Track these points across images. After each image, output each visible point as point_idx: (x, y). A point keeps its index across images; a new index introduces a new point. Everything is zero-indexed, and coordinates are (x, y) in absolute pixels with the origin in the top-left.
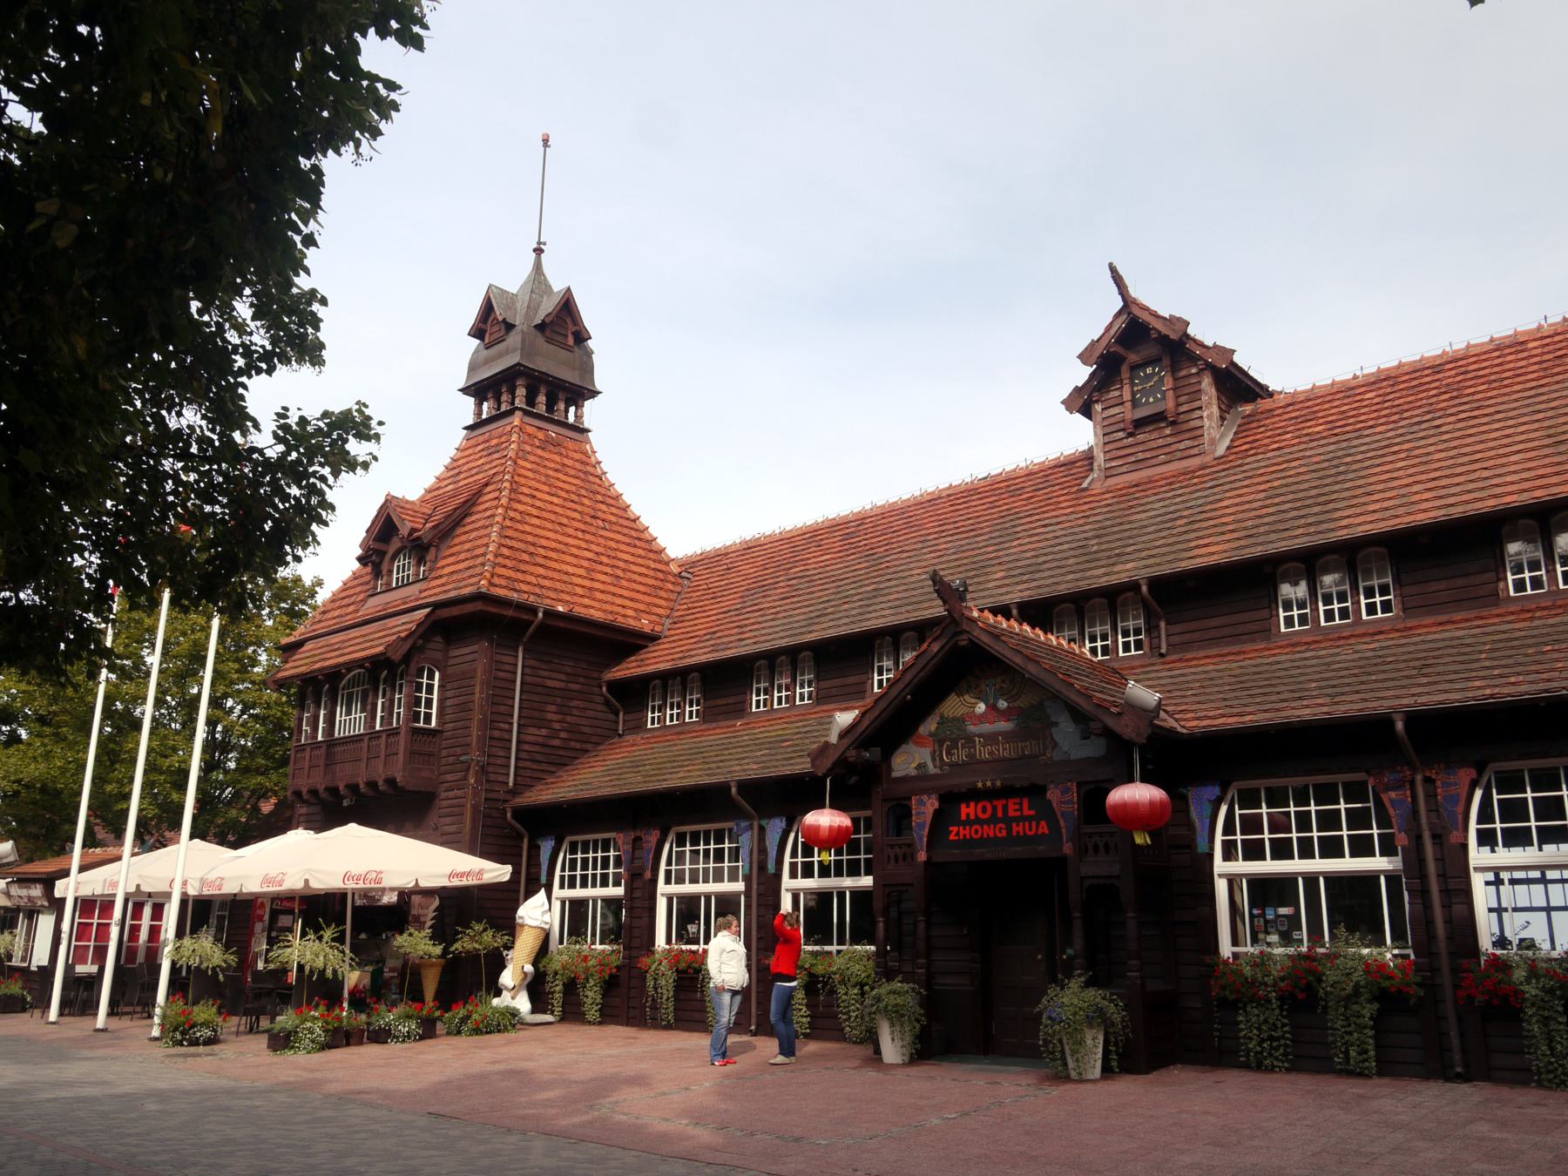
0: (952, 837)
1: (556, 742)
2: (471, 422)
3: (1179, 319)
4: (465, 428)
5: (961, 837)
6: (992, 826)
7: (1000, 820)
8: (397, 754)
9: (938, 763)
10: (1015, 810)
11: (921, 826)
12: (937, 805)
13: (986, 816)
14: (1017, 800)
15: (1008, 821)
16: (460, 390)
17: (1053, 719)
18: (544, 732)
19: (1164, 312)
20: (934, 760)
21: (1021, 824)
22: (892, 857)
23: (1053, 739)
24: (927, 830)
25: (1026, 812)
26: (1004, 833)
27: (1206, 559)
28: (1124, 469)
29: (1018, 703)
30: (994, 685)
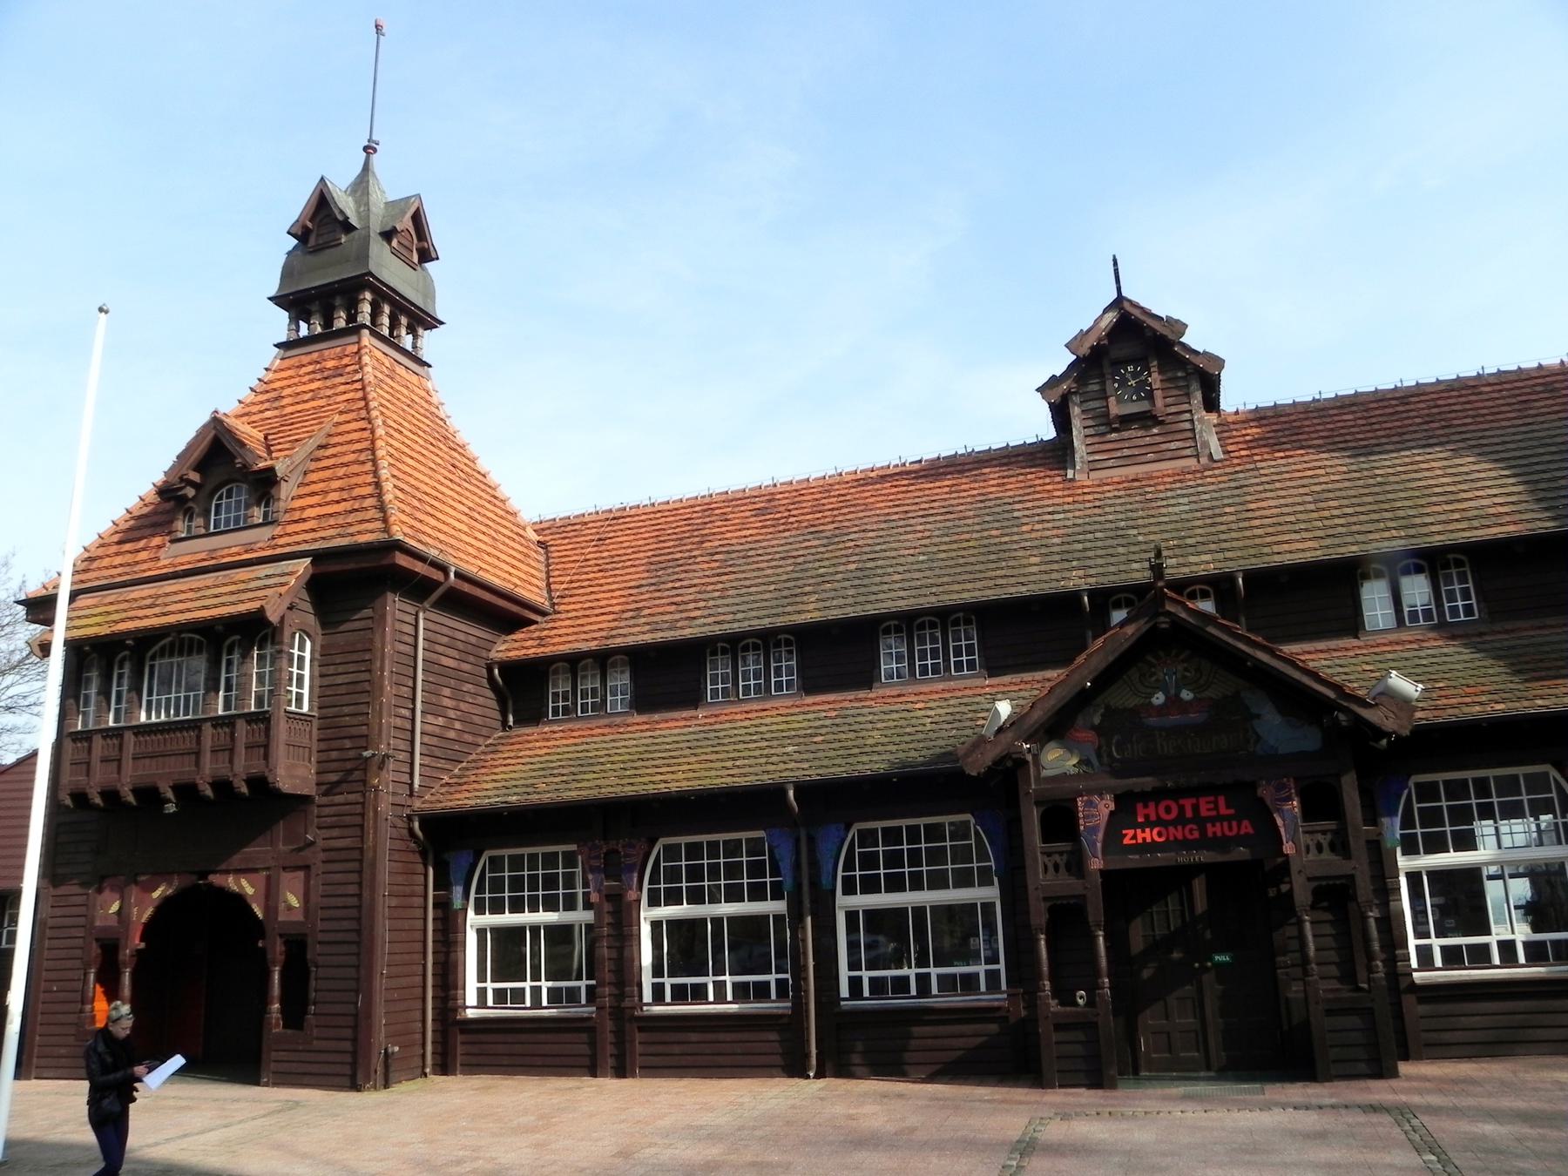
0: (1126, 841)
1: (452, 734)
2: (284, 339)
3: (1177, 321)
4: (277, 346)
5: (1140, 841)
6: (1148, 830)
7: (1190, 821)
8: (318, 740)
9: (1105, 759)
10: (1209, 810)
11: (1094, 829)
12: (1112, 807)
13: (1173, 816)
14: (1212, 798)
15: (1200, 822)
16: (270, 299)
17: (1254, 710)
18: (441, 721)
19: (1162, 312)
20: (1099, 756)
21: (1218, 824)
22: (1050, 866)
23: (1256, 733)
24: (1100, 836)
25: (1224, 811)
26: (1196, 834)
27: (1301, 555)
28: (1110, 463)
29: (1207, 694)
30: (1175, 673)
